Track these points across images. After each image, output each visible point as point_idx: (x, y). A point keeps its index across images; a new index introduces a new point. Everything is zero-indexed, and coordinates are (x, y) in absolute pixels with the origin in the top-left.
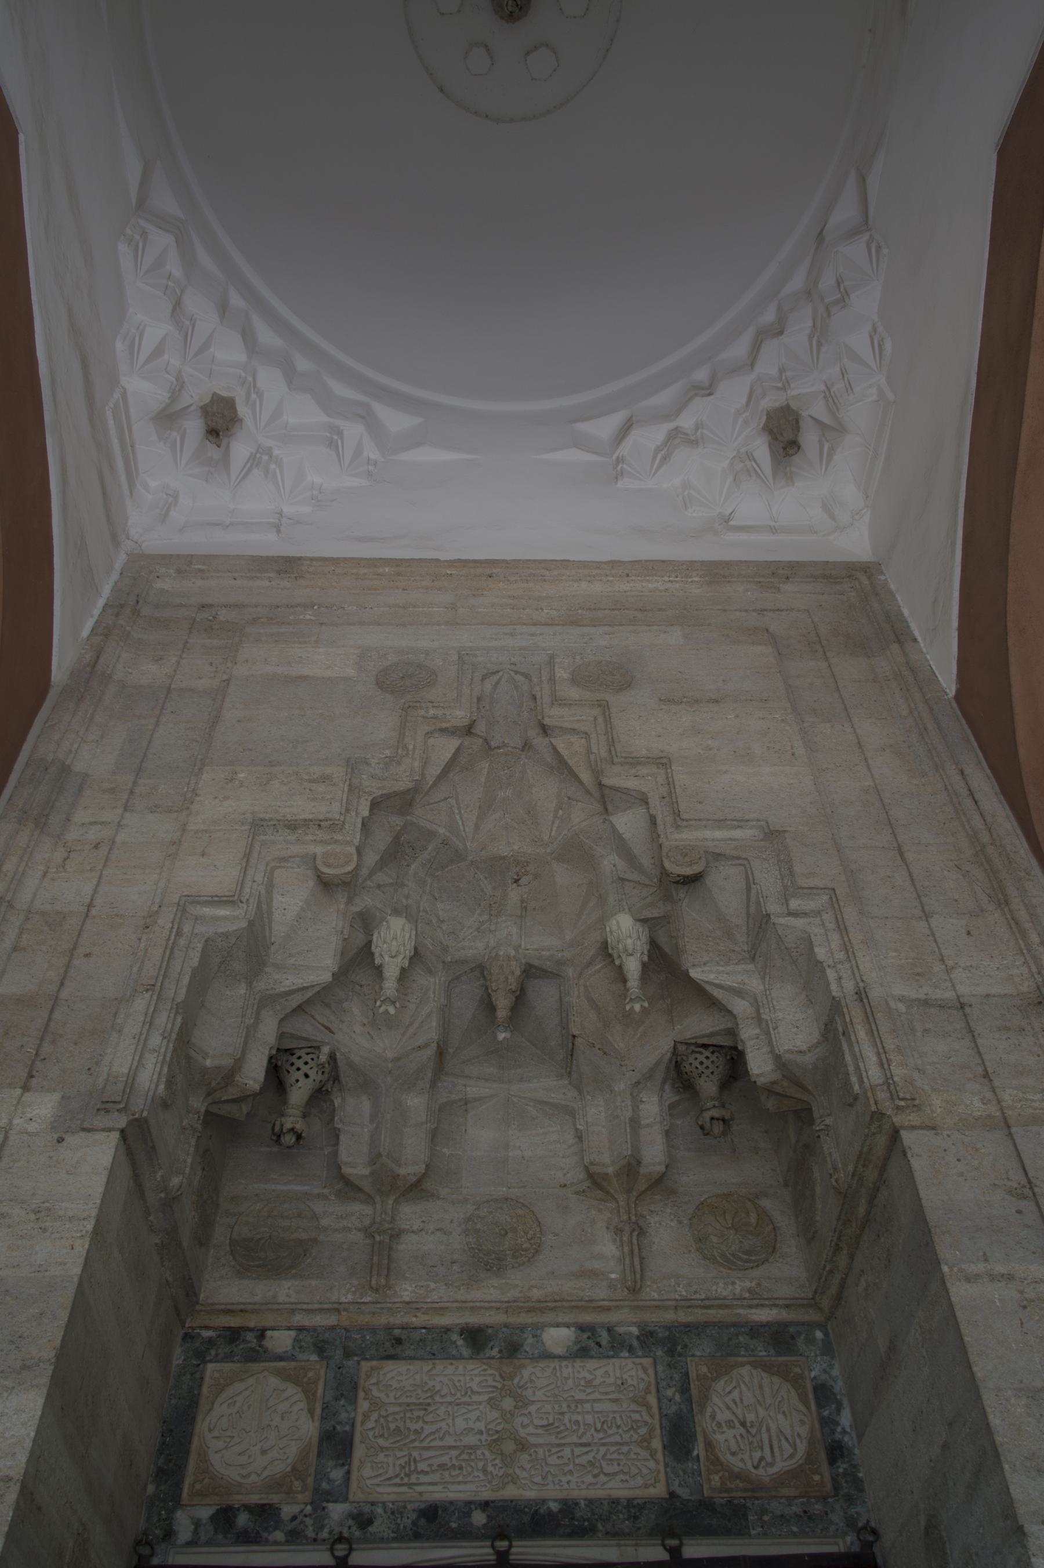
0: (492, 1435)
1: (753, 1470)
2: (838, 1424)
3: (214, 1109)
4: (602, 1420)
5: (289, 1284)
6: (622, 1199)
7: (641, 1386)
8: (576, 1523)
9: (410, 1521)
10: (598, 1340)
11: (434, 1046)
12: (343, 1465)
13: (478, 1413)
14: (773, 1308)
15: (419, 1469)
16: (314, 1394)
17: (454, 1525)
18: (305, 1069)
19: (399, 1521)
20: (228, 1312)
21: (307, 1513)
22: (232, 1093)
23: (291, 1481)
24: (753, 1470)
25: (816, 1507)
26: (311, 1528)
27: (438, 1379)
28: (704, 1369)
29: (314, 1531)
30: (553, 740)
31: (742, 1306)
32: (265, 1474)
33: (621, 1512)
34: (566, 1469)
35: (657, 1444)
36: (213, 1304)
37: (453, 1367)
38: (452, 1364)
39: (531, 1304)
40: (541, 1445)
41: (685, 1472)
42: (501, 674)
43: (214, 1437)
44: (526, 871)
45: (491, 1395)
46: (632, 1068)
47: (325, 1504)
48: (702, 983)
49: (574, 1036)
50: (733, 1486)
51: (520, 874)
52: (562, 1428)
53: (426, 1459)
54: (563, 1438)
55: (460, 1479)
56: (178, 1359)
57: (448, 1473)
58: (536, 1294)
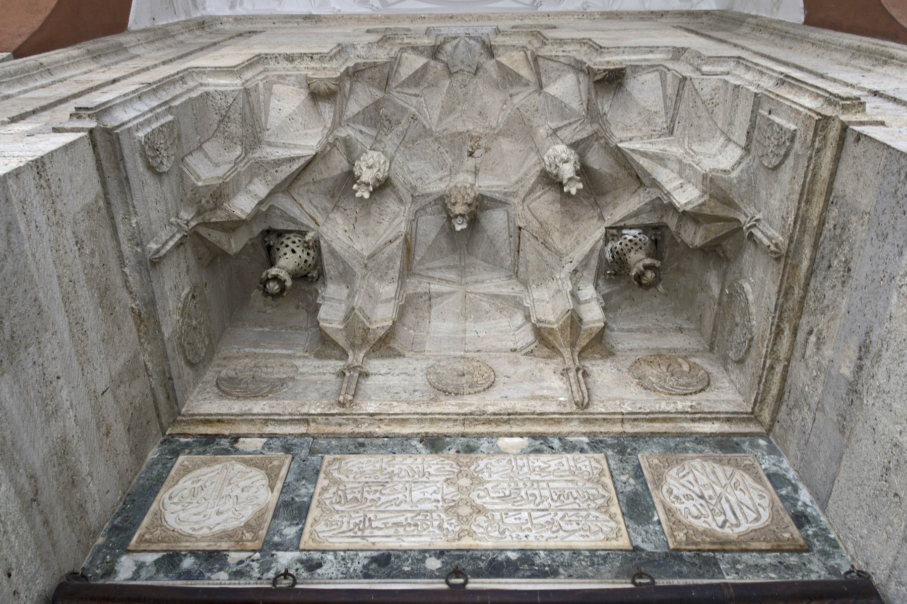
0: (449, 503)
1: (718, 529)
2: (797, 500)
3: (203, 231)
4: (558, 493)
5: (265, 402)
6: (566, 353)
7: (595, 472)
8: (537, 568)
9: (360, 566)
10: (551, 445)
11: (402, 238)
12: (297, 524)
13: (435, 488)
14: (715, 422)
15: (374, 526)
16: (277, 475)
17: (406, 569)
18: (292, 246)
19: (349, 565)
20: (207, 422)
21: (255, 559)
22: (219, 216)
23: (243, 533)
24: (718, 529)
25: (791, 559)
26: (257, 570)
27: (397, 467)
28: (656, 461)
29: (259, 572)
30: (498, 59)
31: (686, 420)
32: (217, 528)
33: (584, 560)
34: (524, 527)
35: (615, 509)
36: (193, 415)
37: (412, 459)
38: (411, 457)
39: (485, 417)
40: (498, 510)
41: (647, 532)
42: (458, 39)
43: (173, 503)
44: (478, 145)
45: (448, 477)
46: (570, 260)
47: (274, 552)
48: (629, 152)
49: (520, 228)
50: (700, 540)
51: (474, 147)
52: (519, 499)
53: (381, 519)
54: (521, 505)
55: (415, 533)
56: (153, 454)
57: (403, 529)
58: (491, 409)
